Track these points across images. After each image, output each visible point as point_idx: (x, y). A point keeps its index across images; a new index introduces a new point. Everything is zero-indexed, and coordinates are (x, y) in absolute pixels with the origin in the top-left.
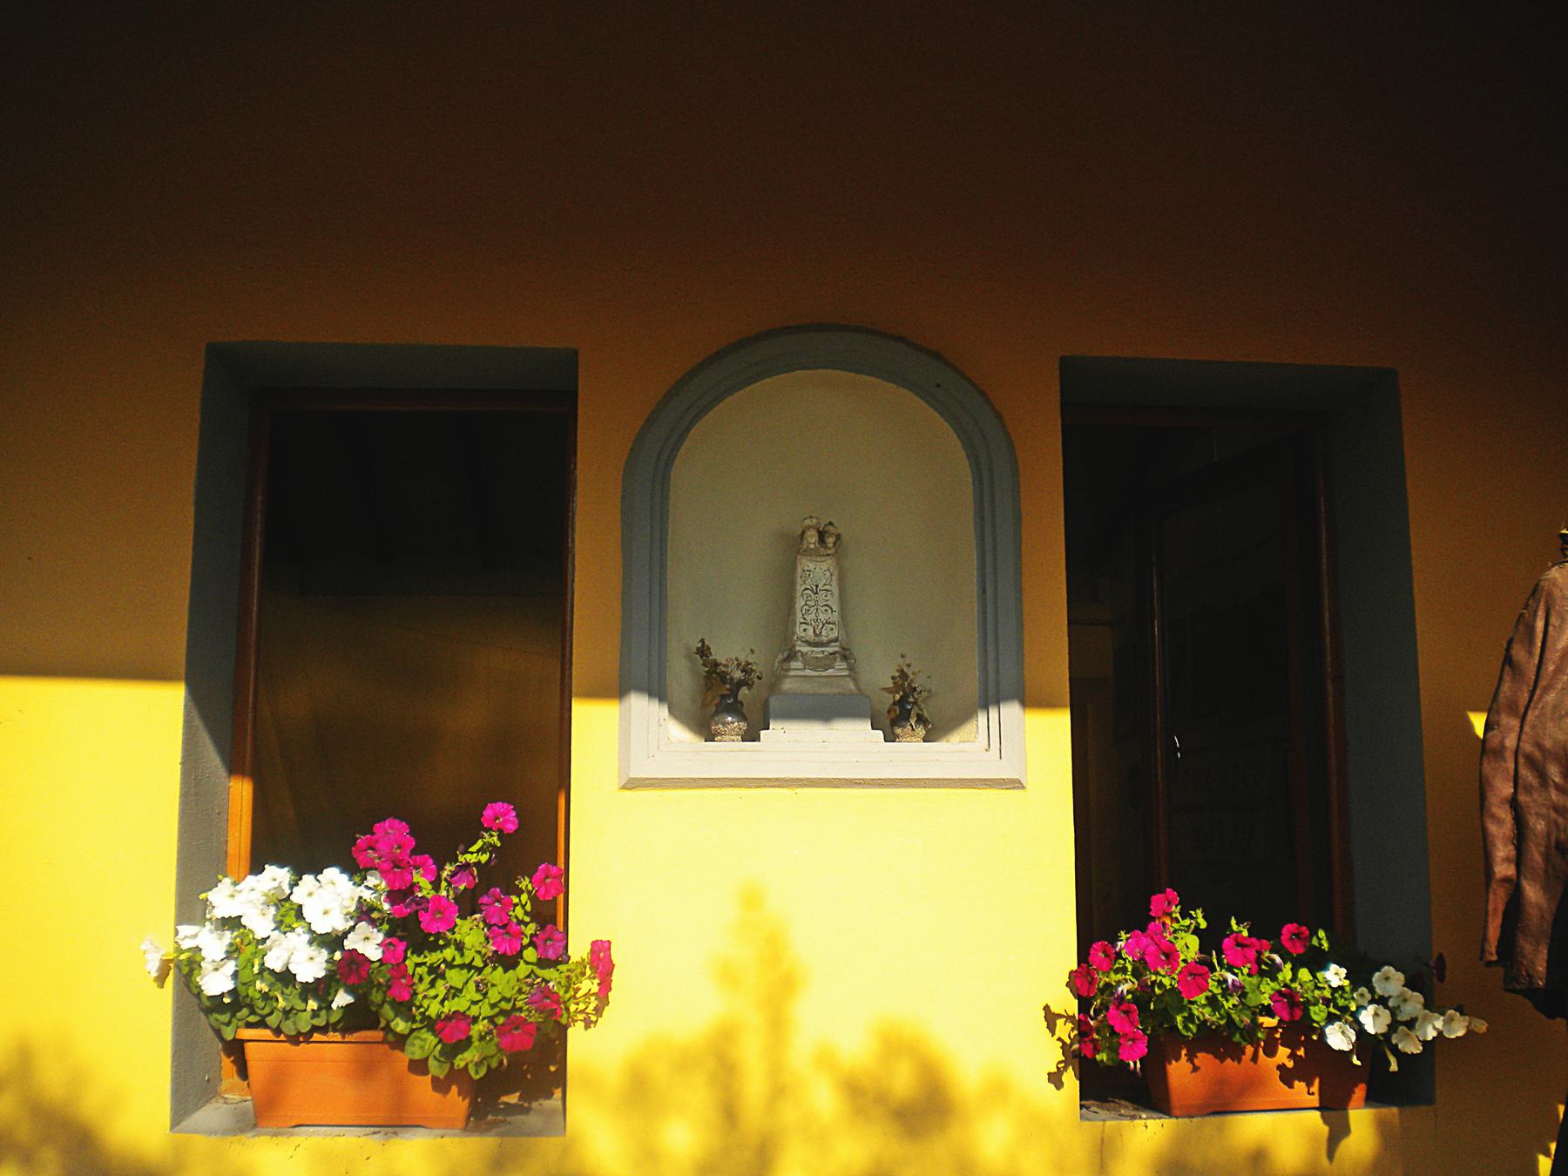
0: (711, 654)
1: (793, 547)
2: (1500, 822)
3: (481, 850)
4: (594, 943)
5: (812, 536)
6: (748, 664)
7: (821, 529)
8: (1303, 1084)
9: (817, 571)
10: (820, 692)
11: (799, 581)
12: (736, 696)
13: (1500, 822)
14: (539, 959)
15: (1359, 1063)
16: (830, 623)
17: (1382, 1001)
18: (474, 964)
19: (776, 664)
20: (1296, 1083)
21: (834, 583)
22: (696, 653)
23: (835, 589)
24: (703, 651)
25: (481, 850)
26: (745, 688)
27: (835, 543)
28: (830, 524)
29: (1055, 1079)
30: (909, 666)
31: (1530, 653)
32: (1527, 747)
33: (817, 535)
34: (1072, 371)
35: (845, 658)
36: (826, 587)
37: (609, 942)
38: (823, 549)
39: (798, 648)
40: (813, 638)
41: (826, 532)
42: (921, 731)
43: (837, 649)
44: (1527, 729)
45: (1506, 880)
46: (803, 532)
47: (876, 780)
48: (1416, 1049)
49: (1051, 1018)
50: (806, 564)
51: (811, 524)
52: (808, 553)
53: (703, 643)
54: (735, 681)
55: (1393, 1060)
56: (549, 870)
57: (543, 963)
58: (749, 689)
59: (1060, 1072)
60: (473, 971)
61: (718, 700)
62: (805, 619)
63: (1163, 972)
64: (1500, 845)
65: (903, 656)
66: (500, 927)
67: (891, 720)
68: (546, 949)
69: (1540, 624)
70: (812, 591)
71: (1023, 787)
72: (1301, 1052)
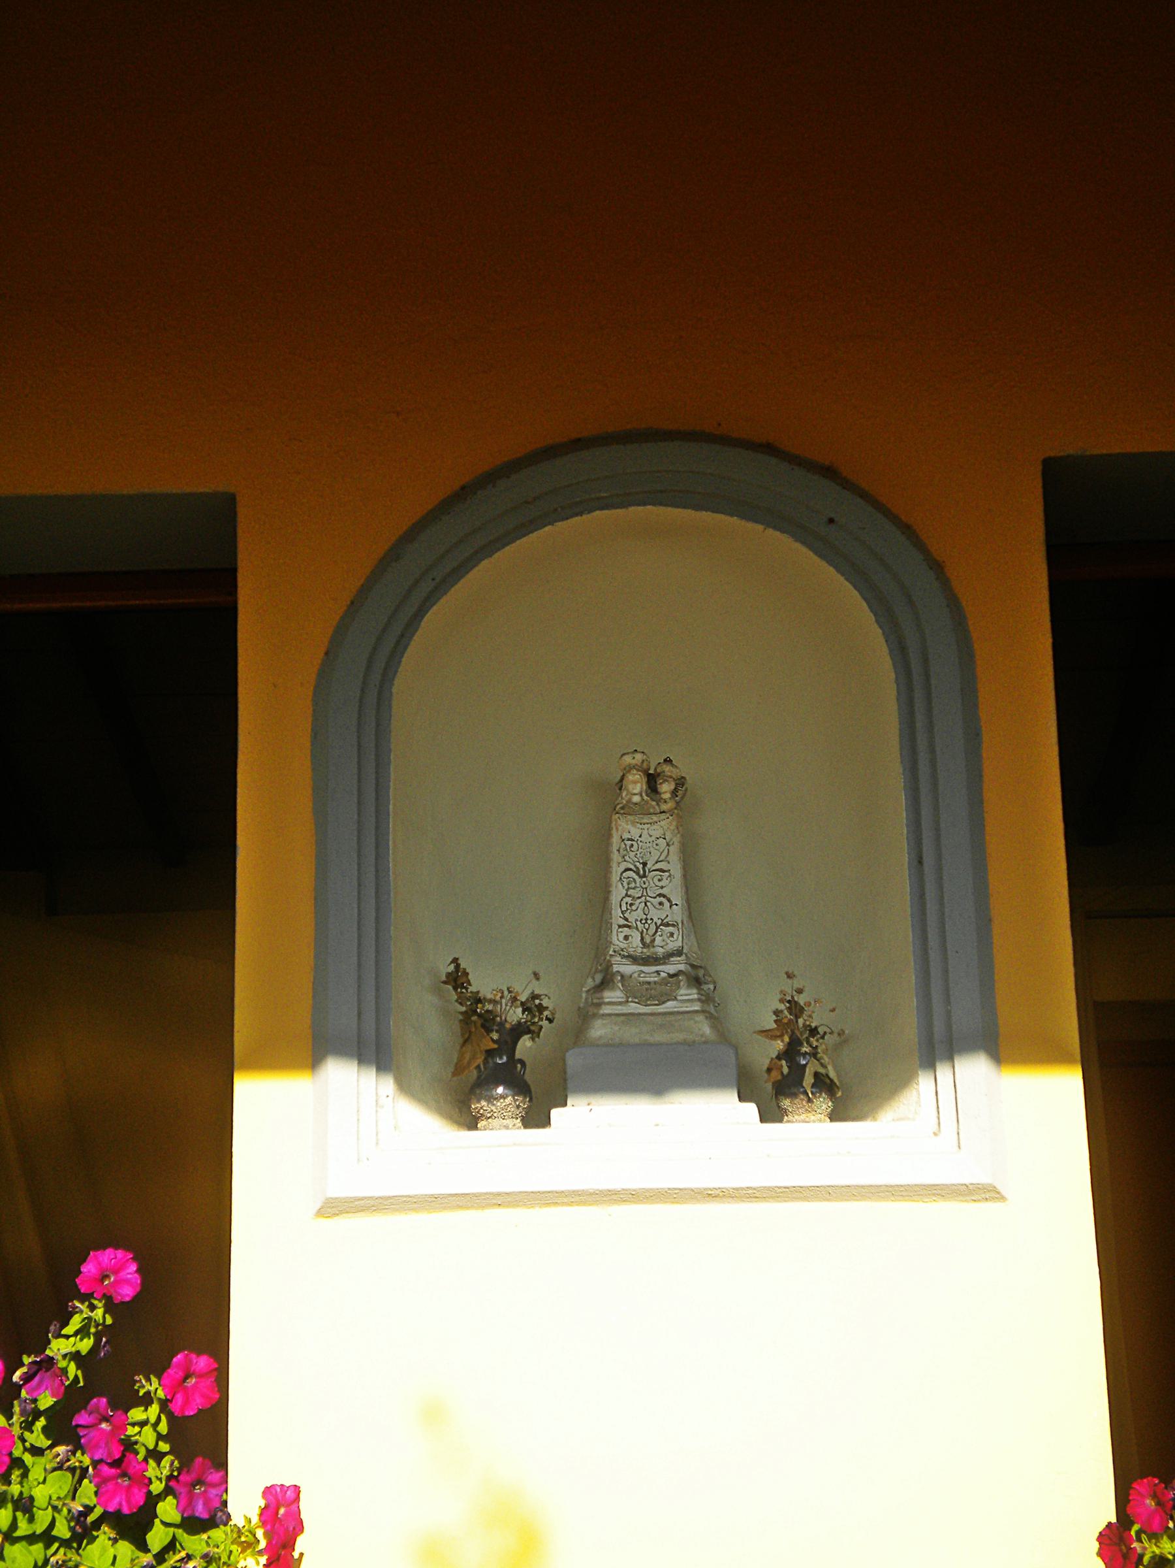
0: (469, 983)
3: (82, 1332)
4: (268, 1491)
5: (635, 782)
6: (534, 997)
7: (651, 771)
10: (651, 1040)
11: (616, 857)
14: (183, 1519)
16: (667, 925)
18: (54, 1533)
19: (584, 995)
21: (674, 857)
22: (445, 983)
24: (455, 980)
25: (82, 1332)
26: (526, 1037)
27: (674, 793)
28: (668, 761)
30: (800, 991)
33: (645, 780)
35: (696, 982)
36: (658, 866)
37: (297, 1489)
38: (654, 803)
39: (615, 968)
40: (640, 950)
41: (659, 775)
42: (823, 1104)
43: (682, 967)
47: (742, 1189)
50: (626, 828)
51: (634, 762)
52: (628, 810)
53: (458, 967)
54: (508, 1026)
56: (191, 1361)
57: (194, 1524)
58: (533, 1039)
60: (56, 1545)
61: (480, 1061)
62: (626, 919)
65: (789, 976)
66: (111, 1465)
67: (774, 1084)
68: (191, 1497)
70: (638, 873)
71: (1002, 1198)
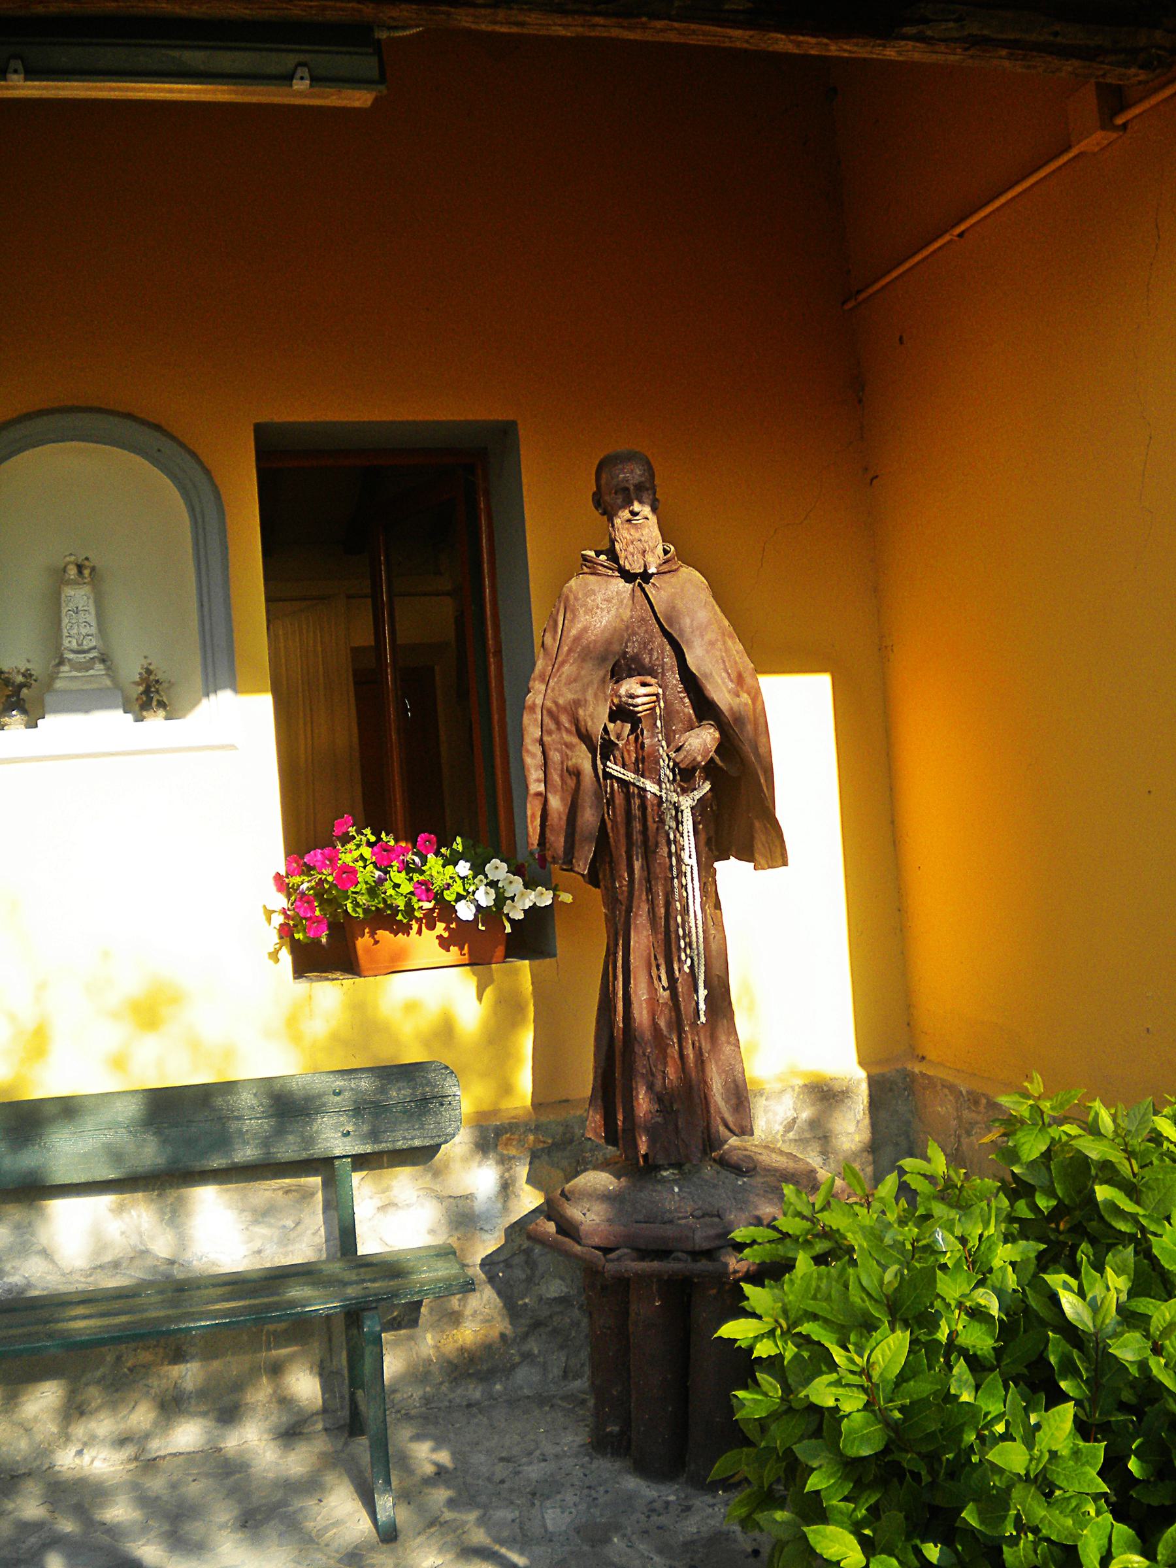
1: (58, 578)
2: (533, 756)
8: (456, 948)
9: (78, 596)
11: (64, 604)
12: (18, 695)
13: (533, 756)
15: (483, 928)
17: (493, 884)
20: (452, 948)
23: (92, 610)
27: (90, 574)
28: (87, 559)
29: (274, 956)
30: (150, 664)
31: (554, 639)
32: (549, 704)
34: (262, 432)
35: (103, 661)
36: (85, 608)
43: (96, 654)
44: (549, 691)
45: (538, 794)
46: (65, 567)
48: (520, 916)
49: (269, 914)
50: (68, 591)
52: (69, 583)
55: (508, 925)
59: (277, 951)
63: (325, 872)
64: (533, 771)
65: (145, 657)
69: (561, 619)
72: (453, 926)
